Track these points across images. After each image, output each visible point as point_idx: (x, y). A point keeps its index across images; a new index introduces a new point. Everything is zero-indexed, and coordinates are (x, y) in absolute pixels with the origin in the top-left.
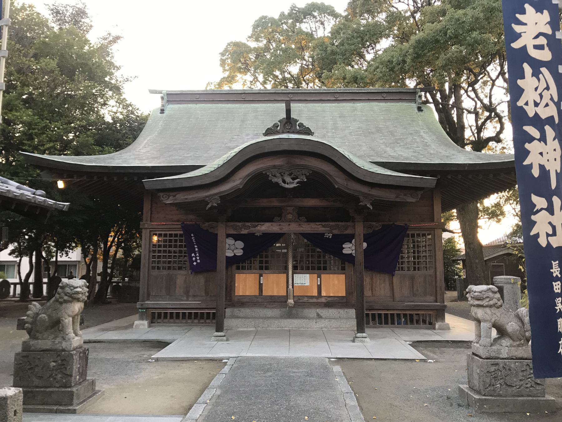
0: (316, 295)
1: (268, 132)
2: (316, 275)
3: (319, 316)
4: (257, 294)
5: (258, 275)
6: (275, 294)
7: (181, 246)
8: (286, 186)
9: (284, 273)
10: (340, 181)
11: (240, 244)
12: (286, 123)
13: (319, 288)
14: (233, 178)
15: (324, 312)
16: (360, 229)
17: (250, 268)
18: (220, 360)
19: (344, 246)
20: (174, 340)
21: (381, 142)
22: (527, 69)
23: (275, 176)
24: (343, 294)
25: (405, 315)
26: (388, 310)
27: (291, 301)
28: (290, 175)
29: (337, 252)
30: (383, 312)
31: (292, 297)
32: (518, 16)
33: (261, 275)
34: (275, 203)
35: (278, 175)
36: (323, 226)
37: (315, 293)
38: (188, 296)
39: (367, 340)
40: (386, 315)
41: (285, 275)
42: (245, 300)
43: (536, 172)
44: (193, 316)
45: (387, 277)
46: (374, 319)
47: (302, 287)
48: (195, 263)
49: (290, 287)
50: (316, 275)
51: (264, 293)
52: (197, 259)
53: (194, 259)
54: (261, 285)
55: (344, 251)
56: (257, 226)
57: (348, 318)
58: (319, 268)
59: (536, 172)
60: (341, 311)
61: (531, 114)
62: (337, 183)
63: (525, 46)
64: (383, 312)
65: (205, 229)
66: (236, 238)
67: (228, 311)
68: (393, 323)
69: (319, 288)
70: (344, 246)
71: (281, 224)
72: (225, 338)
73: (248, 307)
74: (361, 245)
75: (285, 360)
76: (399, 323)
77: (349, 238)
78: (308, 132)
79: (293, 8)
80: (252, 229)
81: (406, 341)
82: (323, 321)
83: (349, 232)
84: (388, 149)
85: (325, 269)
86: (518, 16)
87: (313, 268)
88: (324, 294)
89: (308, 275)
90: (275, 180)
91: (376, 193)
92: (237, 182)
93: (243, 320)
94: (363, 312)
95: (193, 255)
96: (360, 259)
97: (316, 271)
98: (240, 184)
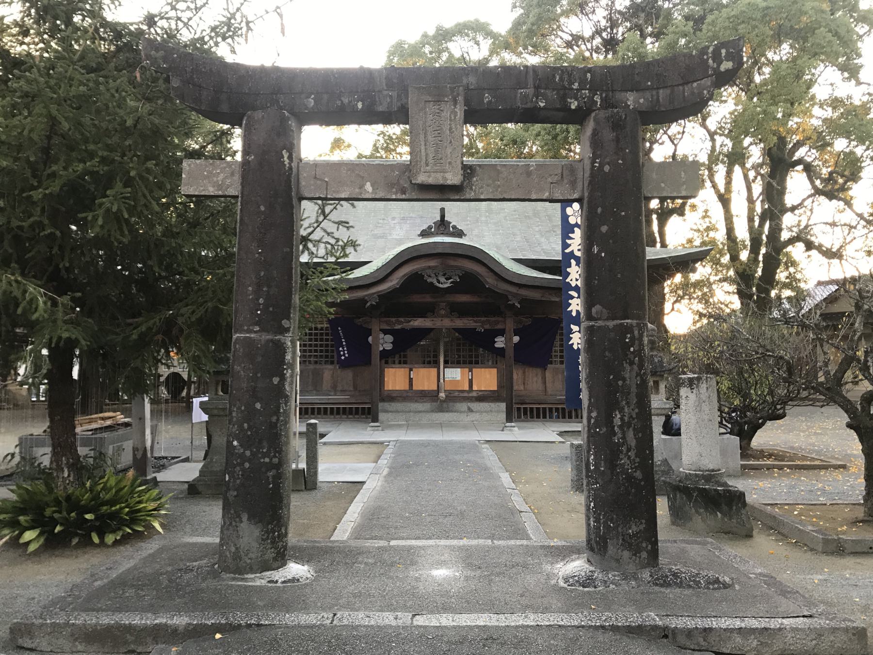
0: (468, 389)
1: (424, 234)
2: (467, 370)
3: (470, 410)
4: (407, 388)
5: (408, 369)
6: (426, 389)
7: (327, 340)
8: (441, 286)
9: (435, 367)
10: (490, 281)
11: (389, 338)
12: (440, 225)
14: (390, 278)
15: (475, 406)
16: (510, 325)
17: (394, 363)
18: (382, 443)
19: (496, 340)
20: (329, 432)
21: (537, 229)
22: (573, 262)
23: (430, 276)
24: (495, 388)
25: (557, 410)
26: (539, 404)
27: (442, 395)
28: (444, 275)
29: (489, 345)
30: (535, 406)
31: (443, 391)
32: (570, 235)
33: (411, 370)
34: (428, 299)
35: (433, 275)
36: (475, 322)
37: (466, 388)
38: (335, 391)
39: (516, 429)
40: (538, 409)
41: (436, 369)
42: (394, 395)
43: (574, 314)
44: (341, 411)
45: (539, 371)
46: (525, 414)
48: (343, 358)
49: (442, 381)
50: (467, 370)
51: (415, 388)
52: (344, 353)
53: (342, 353)
54: (411, 380)
55: (497, 345)
56: (410, 321)
57: (498, 412)
58: (471, 363)
59: (574, 314)
60: (492, 405)
61: (573, 285)
62: (488, 283)
63: (573, 251)
64: (535, 406)
65: (359, 324)
66: (386, 332)
67: (381, 405)
68: (545, 417)
70: (496, 340)
71: (435, 319)
72: (380, 428)
73: (398, 401)
74: (511, 339)
75: (440, 441)
76: (551, 417)
77: (502, 333)
78: (460, 234)
79: (439, 29)
80: (405, 324)
81: (554, 431)
82: (474, 414)
83: (500, 327)
84: (543, 240)
85: (477, 363)
86: (570, 235)
87: (465, 362)
88: (475, 388)
89: (459, 369)
90: (430, 280)
91: (524, 292)
92: (393, 282)
93: (394, 414)
94: (512, 406)
95: (341, 349)
96: (510, 353)
97: (467, 365)
98: (397, 284)
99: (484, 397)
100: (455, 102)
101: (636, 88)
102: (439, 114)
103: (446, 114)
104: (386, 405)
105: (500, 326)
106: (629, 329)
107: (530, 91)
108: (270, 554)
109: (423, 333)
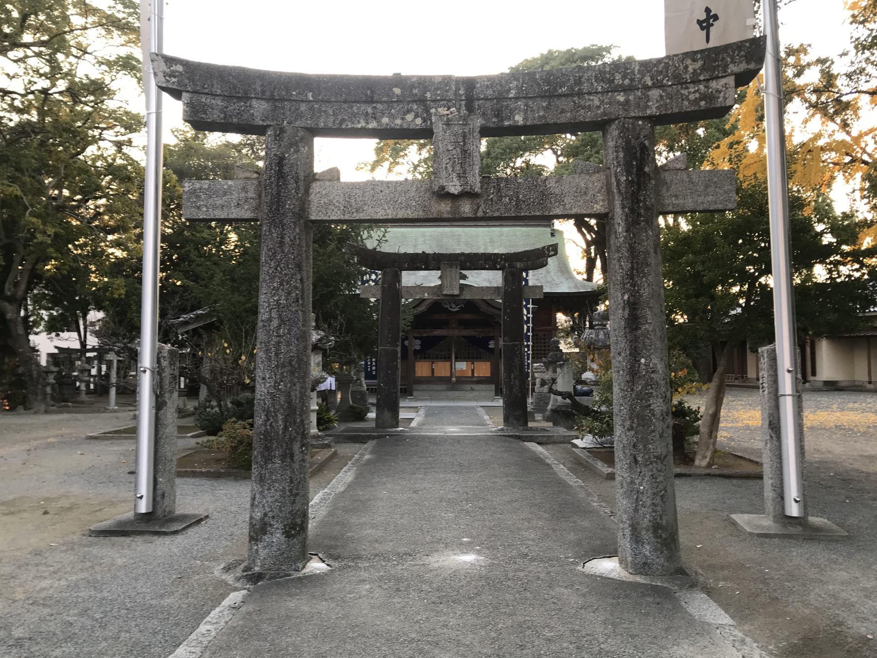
3: (472, 390)
11: (418, 342)
13: (473, 371)
15: (475, 387)
27: (454, 379)
29: (485, 346)
33: (433, 363)
37: (470, 375)
47: (462, 371)
54: (433, 370)
58: (473, 358)
66: (416, 338)
69: (473, 371)
87: (469, 358)
88: (476, 375)
90: (445, 306)
99: (481, 381)
100: (461, 186)
101: (521, 261)
102: (451, 271)
103: (454, 271)
104: (415, 386)
105: (491, 335)
106: (517, 345)
107: (483, 262)
108: (394, 423)
109: (442, 338)
